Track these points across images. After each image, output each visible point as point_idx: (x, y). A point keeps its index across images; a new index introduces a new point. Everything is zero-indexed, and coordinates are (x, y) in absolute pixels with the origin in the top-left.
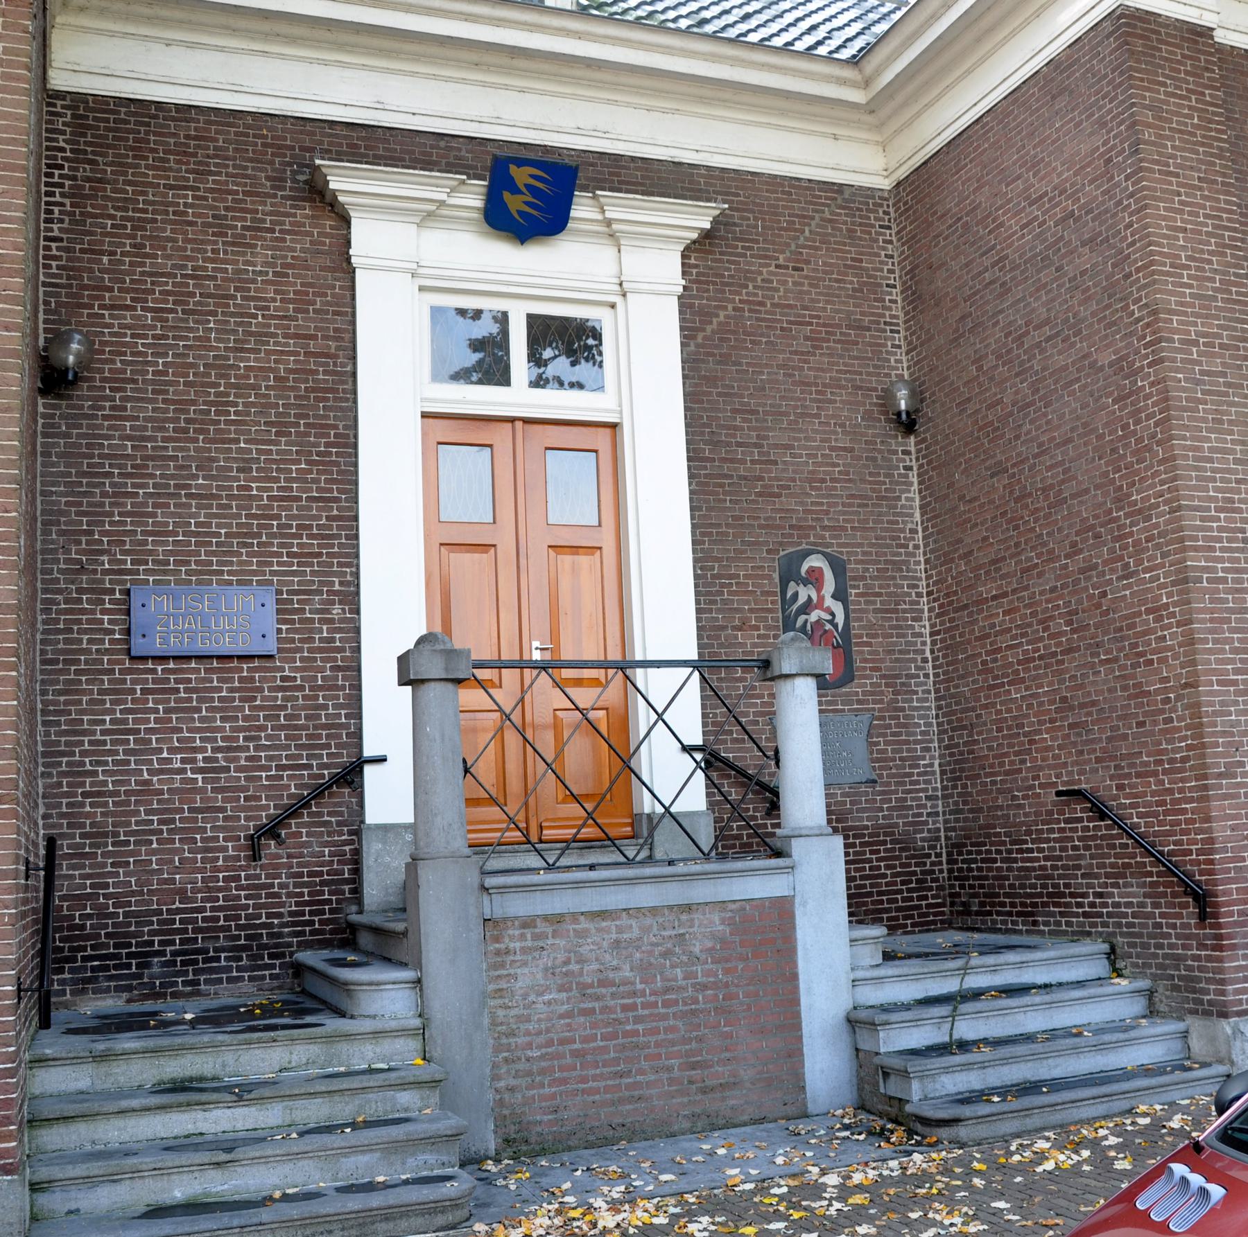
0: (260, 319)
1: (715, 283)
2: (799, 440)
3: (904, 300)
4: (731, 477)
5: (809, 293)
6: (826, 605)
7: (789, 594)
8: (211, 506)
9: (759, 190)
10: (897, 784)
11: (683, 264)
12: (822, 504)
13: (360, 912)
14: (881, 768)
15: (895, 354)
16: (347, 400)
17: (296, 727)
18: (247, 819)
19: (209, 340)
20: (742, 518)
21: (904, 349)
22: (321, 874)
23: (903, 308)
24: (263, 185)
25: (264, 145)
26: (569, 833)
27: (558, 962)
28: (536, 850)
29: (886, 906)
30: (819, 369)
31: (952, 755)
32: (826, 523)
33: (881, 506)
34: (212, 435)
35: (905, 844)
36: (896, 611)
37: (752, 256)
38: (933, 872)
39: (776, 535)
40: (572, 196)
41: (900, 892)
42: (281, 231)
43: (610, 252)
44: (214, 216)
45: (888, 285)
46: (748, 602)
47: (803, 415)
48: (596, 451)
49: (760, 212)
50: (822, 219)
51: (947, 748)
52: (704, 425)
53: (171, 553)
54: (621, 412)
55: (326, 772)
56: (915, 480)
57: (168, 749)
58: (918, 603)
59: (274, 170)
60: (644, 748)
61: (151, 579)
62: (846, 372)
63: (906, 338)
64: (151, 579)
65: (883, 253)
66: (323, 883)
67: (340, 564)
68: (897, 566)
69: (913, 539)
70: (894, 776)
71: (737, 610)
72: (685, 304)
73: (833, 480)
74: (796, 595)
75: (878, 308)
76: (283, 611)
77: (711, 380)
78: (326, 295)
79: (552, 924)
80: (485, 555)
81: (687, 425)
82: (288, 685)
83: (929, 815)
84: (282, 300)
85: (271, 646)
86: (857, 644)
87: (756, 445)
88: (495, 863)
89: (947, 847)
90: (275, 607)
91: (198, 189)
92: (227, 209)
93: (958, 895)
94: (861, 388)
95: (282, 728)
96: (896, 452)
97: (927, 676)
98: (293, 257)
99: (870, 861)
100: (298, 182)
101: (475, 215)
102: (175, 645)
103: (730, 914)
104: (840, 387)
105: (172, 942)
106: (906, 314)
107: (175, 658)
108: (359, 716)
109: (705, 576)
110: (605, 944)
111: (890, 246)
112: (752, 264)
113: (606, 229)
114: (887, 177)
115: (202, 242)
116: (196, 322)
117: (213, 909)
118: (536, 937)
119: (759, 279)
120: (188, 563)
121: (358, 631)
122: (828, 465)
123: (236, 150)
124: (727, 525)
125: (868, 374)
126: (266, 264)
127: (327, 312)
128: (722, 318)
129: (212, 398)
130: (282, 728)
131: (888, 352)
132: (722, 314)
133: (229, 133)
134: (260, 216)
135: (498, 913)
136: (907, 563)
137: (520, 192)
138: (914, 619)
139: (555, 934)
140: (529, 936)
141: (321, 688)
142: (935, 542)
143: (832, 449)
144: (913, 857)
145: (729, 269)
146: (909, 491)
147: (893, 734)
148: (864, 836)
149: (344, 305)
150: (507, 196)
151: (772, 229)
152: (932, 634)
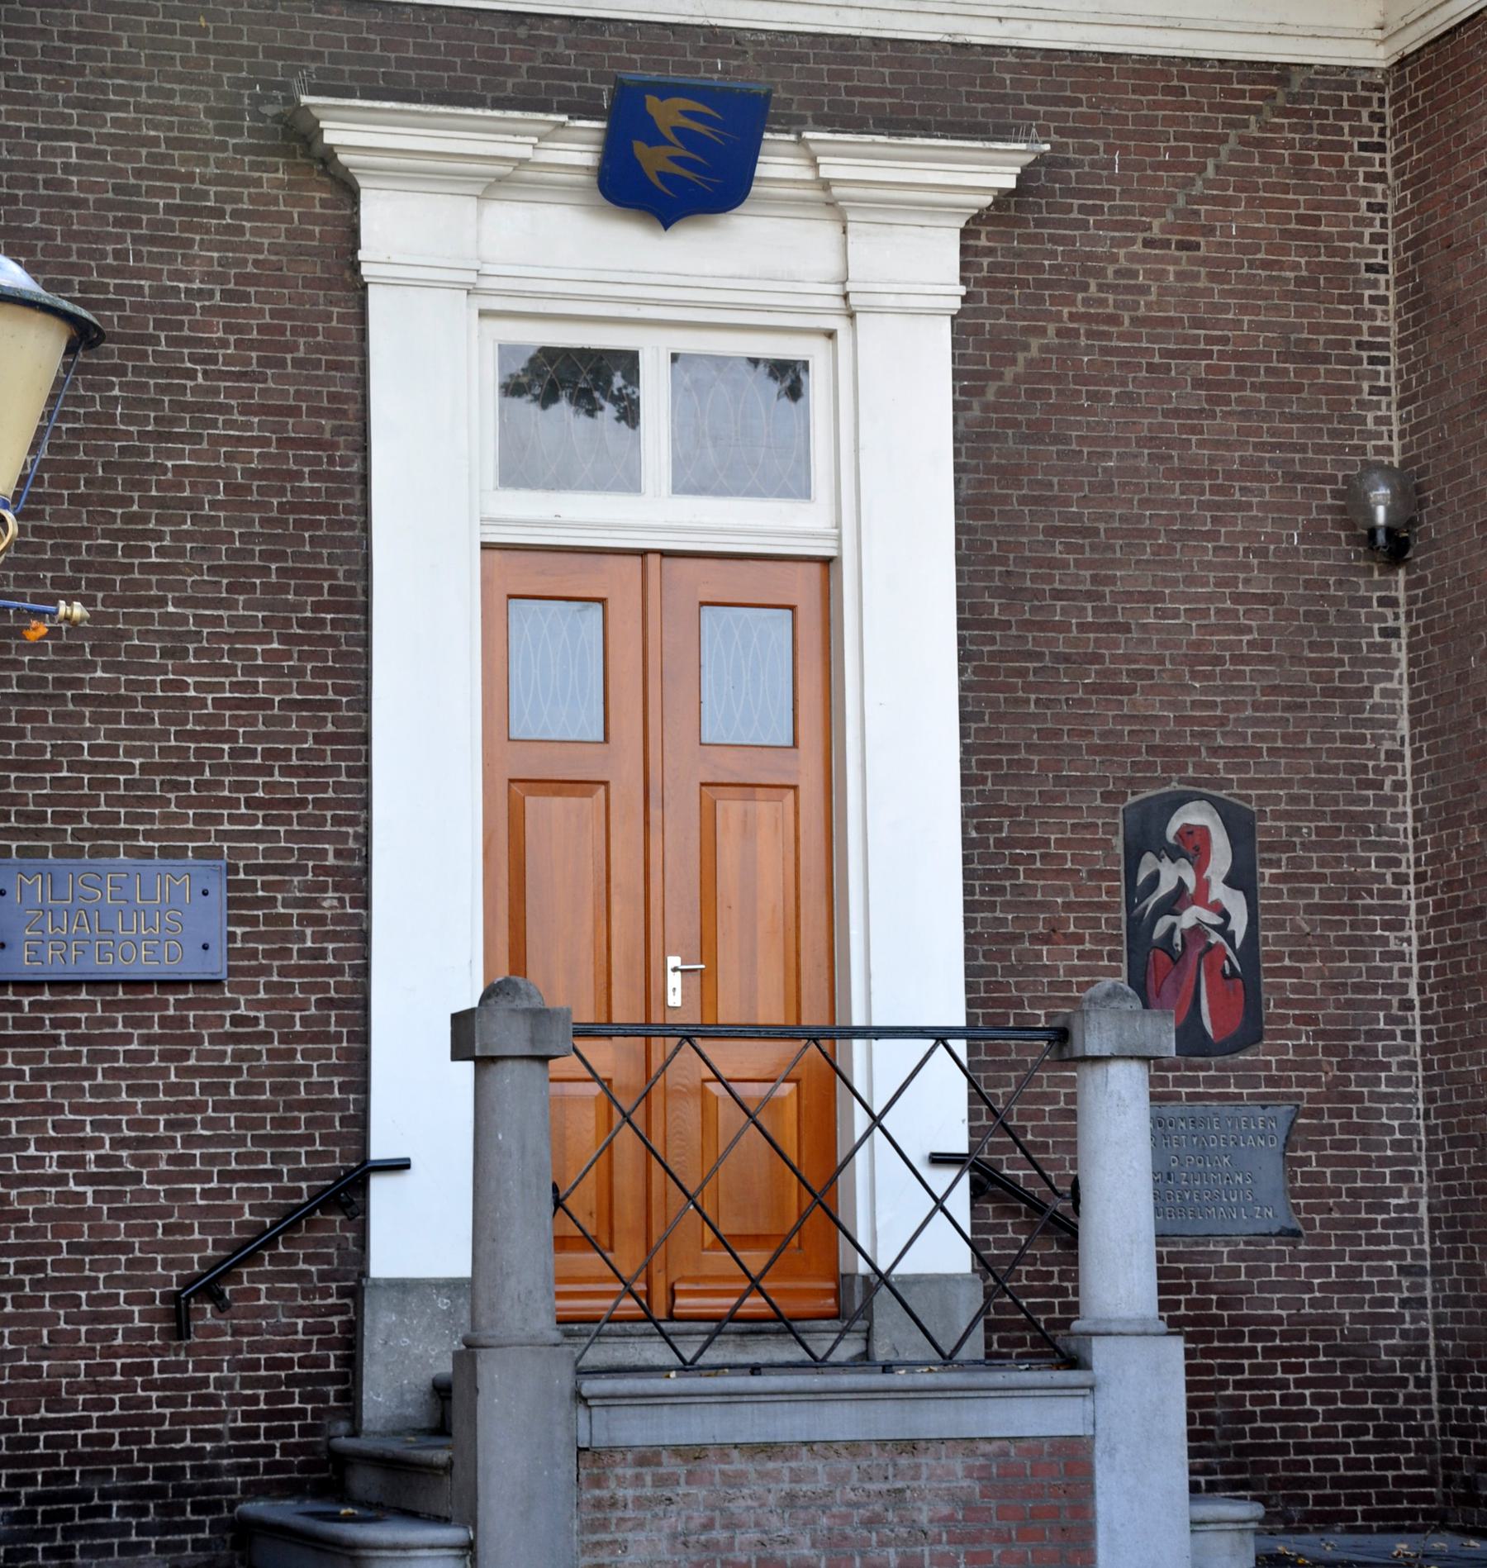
0: (200, 379)
1: (1023, 284)
2: (1174, 582)
3: (1400, 297)
4: (1039, 656)
5: (1209, 292)
6: (1212, 897)
7: (1142, 876)
8: (115, 718)
9: (1121, 89)
10: (1341, 1240)
11: (964, 250)
12: (1213, 705)
13: (355, 1433)
14: (1309, 1209)
15: (1377, 405)
16: (351, 526)
17: (256, 1106)
18: (168, 1265)
19: (111, 419)
20: (1057, 733)
21: (1395, 395)
22: (288, 1364)
23: (1398, 314)
24: (201, 127)
25: (202, 47)
26: (722, 1305)
27: (695, 1524)
28: (662, 1333)
29: (1312, 1473)
30: (1217, 444)
31: (1449, 1191)
32: (1220, 741)
33: (1330, 707)
34: (118, 592)
35: (1357, 1356)
36: (1352, 910)
37: (1099, 225)
38: (1411, 1415)
39: (1122, 766)
40: (759, 141)
41: (1343, 1448)
42: (235, 214)
43: (828, 231)
44: (117, 189)
45: (1370, 268)
46: (1062, 891)
47: (1184, 534)
48: (792, 608)
49: (1120, 135)
50: (1243, 141)
51: (1443, 1176)
52: (994, 560)
53: (49, 800)
54: (839, 538)
55: (304, 1185)
56: (1403, 656)
57: (37, 1141)
58: (1397, 894)
59: (221, 96)
60: (861, 1156)
61: (14, 845)
62: (1274, 447)
63: (1399, 372)
64: (14, 845)
65: (1364, 201)
66: (292, 1380)
67: (337, 820)
68: (1358, 823)
69: (1394, 771)
70: (1335, 1224)
71: (1042, 906)
72: (963, 329)
73: (1238, 659)
74: (1155, 879)
75: (1346, 314)
76: (239, 902)
77: (1010, 474)
78: (314, 332)
79: (686, 1461)
80: (587, 801)
81: (959, 561)
82: (243, 1033)
83: (1404, 1303)
84: (239, 344)
85: (215, 965)
86: (1272, 972)
87: (1090, 596)
88: (597, 1356)
89: (1439, 1369)
90: (225, 895)
91: (87, 137)
92: (138, 173)
93: (1456, 1464)
94: (1301, 477)
95: (231, 1106)
96: (1366, 602)
97: (1409, 1035)
98: (256, 263)
99: (1283, 1384)
100: (261, 117)
101: (582, 178)
102: (52, 965)
103: (981, 1461)
104: (1259, 477)
105: (30, 1480)
106: (1403, 326)
107: (53, 984)
108: (364, 1088)
109: (983, 843)
110: (771, 1499)
111: (1379, 187)
112: (1095, 241)
113: (820, 194)
114: (1383, 42)
115: (99, 237)
116: (89, 386)
117: (102, 1423)
118: (660, 1481)
119: (1110, 272)
120: (77, 817)
121: (365, 937)
122: (1228, 629)
123: (151, 59)
124: (1030, 748)
125: (1319, 449)
126: (209, 277)
127: (317, 364)
128: (1034, 352)
129: (118, 525)
130: (231, 1106)
131: (1361, 404)
132: (1035, 343)
133: (138, 26)
134: (197, 185)
135: (601, 1439)
136: (1378, 817)
137: (667, 142)
138: (1387, 926)
139: (691, 1478)
140: (648, 1479)
141: (299, 1038)
142: (1433, 780)
143: (1237, 598)
144: (1370, 1382)
145: (1052, 255)
146: (1390, 678)
147: (1337, 1145)
148: (1272, 1336)
149: (347, 350)
150: (640, 149)
151: (1139, 166)
152: (1423, 956)
